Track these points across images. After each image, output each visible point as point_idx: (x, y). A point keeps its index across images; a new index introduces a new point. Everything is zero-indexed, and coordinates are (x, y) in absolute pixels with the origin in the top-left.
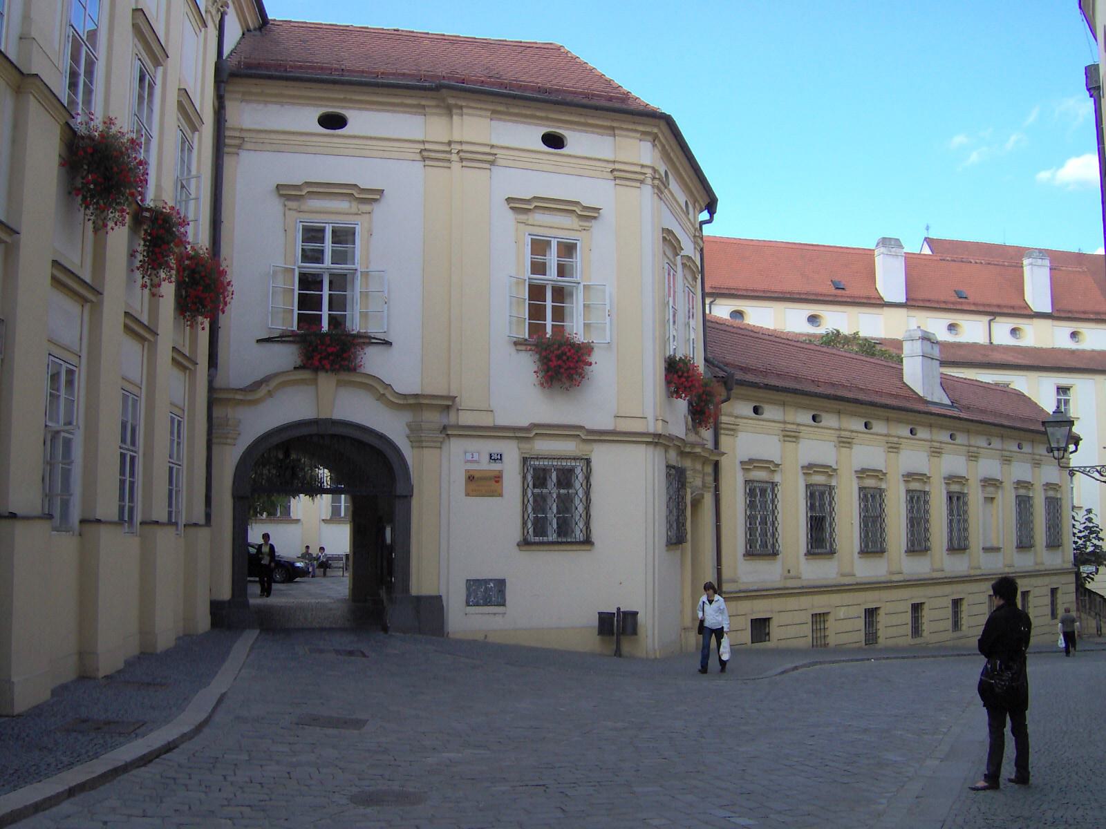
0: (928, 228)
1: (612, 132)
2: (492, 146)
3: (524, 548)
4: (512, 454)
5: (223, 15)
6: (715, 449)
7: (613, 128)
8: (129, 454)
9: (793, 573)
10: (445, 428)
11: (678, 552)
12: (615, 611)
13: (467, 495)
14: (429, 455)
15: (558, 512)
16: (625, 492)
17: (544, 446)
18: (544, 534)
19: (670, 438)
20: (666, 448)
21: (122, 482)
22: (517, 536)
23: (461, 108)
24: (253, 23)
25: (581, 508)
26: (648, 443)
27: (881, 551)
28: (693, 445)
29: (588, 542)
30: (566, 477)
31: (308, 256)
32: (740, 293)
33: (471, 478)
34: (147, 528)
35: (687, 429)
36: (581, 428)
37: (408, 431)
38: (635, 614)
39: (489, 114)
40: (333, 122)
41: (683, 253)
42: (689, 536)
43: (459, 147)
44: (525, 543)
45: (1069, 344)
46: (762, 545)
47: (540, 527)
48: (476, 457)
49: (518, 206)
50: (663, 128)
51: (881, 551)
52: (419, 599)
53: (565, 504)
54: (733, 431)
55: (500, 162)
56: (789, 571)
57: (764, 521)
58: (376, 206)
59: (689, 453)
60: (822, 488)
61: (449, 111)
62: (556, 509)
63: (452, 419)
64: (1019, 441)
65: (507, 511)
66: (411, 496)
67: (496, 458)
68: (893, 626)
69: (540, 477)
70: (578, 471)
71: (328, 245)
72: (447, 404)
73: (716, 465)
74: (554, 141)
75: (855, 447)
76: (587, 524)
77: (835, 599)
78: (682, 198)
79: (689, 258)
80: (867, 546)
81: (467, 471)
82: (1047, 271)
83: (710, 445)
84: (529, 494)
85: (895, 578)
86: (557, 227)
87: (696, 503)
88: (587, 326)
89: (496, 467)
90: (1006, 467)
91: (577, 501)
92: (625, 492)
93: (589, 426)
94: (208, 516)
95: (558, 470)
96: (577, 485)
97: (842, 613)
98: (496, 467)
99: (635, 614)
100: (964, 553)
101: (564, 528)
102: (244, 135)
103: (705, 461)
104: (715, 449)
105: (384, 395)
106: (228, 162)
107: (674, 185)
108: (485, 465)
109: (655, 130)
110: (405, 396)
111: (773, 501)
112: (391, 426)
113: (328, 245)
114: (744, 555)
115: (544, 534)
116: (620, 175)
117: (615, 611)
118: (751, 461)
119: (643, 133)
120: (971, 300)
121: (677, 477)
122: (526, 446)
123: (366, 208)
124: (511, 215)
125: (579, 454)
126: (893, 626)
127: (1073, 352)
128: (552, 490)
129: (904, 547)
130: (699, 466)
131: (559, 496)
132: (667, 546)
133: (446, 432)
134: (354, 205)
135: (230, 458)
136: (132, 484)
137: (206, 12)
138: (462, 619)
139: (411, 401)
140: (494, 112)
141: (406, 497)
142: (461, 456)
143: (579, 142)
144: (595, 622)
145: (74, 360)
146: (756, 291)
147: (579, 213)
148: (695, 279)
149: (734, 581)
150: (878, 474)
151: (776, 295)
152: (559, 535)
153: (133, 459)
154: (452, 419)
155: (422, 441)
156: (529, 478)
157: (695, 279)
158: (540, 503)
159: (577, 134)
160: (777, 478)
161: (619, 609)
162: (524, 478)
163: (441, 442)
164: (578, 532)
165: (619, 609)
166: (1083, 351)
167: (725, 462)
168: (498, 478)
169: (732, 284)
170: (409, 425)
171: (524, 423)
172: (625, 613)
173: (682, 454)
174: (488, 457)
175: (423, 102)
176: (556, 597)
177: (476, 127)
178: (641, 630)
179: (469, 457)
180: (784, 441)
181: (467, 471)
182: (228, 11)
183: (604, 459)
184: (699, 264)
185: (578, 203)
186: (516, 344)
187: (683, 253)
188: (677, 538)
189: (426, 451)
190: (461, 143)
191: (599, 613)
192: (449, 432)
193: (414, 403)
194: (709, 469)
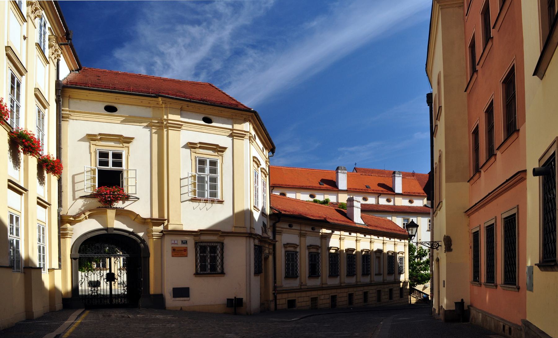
0: (356, 164)
4: (191, 241)
5: (58, 60)
8: (42, 246)
9: (304, 284)
11: (259, 277)
13: (173, 256)
15: (210, 262)
17: (204, 238)
18: (205, 271)
19: (256, 235)
20: (254, 239)
21: (40, 256)
22: (194, 272)
25: (219, 261)
26: (246, 237)
28: (265, 238)
29: (222, 273)
30: (213, 249)
31: (101, 163)
33: (174, 250)
38: (242, 299)
41: (261, 167)
42: (263, 271)
44: (197, 274)
45: (410, 205)
46: (291, 273)
47: (203, 268)
48: (176, 242)
53: (214, 259)
54: (280, 233)
65: (188, 263)
67: (185, 242)
68: (372, 297)
70: (218, 247)
71: (110, 159)
73: (274, 246)
76: (222, 266)
77: (320, 292)
78: (261, 146)
79: (263, 169)
81: (172, 247)
82: (401, 178)
83: (271, 238)
84: (198, 255)
86: (208, 155)
87: (266, 258)
91: (218, 258)
92: (238, 256)
95: (210, 246)
96: (218, 252)
97: (322, 297)
99: (242, 299)
103: (270, 244)
106: (63, 123)
107: (257, 140)
108: (180, 245)
111: (296, 258)
113: (110, 159)
115: (205, 271)
118: (288, 244)
120: (372, 188)
121: (259, 250)
122: (197, 238)
126: (372, 297)
127: (409, 207)
130: (267, 246)
131: (210, 256)
135: (69, 243)
136: (44, 256)
137: (49, 58)
138: (171, 302)
145: (44, 224)
148: (266, 177)
149: (281, 287)
152: (211, 271)
153: (43, 248)
156: (198, 249)
157: (266, 177)
160: (298, 250)
162: (196, 250)
164: (218, 269)
166: (413, 207)
167: (278, 245)
168: (185, 250)
169: (280, 183)
172: (238, 299)
173: (260, 241)
176: (209, 292)
179: (173, 242)
181: (172, 247)
182: (60, 58)
183: (229, 242)
184: (267, 171)
187: (261, 167)
188: (258, 271)
194: (271, 247)
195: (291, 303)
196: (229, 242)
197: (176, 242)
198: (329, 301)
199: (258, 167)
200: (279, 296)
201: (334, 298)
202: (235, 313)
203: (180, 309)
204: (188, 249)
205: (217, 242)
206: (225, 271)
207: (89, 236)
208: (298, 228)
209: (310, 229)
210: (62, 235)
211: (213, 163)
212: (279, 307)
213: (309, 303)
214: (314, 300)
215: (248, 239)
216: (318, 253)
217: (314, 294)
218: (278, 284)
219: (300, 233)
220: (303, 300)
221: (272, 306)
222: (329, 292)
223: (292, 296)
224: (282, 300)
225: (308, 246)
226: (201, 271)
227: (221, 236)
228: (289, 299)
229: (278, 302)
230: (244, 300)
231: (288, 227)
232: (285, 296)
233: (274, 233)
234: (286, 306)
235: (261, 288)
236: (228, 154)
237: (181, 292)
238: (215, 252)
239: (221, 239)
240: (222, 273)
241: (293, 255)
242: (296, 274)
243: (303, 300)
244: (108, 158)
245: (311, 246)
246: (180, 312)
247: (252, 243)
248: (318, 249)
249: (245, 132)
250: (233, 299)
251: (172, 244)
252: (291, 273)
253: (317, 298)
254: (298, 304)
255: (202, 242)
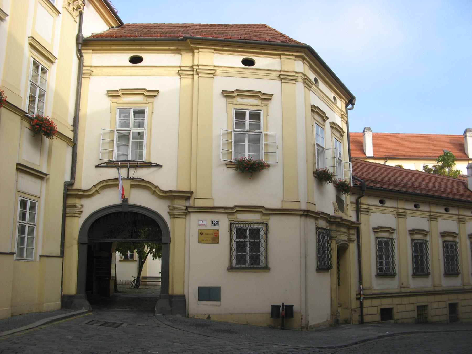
1: (279, 57)
2: (214, 66)
3: (230, 271)
6: (117, 186)
7: (280, 55)
9: (405, 284)
10: (187, 208)
11: (329, 273)
12: (281, 305)
14: (179, 222)
16: (288, 242)
17: (241, 217)
20: (316, 219)
22: (227, 265)
23: (198, 49)
24: (114, 24)
26: (301, 215)
27: (427, 275)
29: (266, 268)
30: (255, 233)
32: (399, 157)
34: (42, 258)
35: (335, 209)
36: (262, 207)
37: (168, 210)
38: (293, 306)
39: (213, 51)
40: (136, 60)
43: (197, 68)
44: (231, 268)
46: (385, 270)
47: (241, 259)
48: (204, 223)
49: (227, 95)
50: (307, 53)
51: (427, 275)
52: (172, 296)
53: (255, 247)
54: (367, 212)
55: (217, 74)
56: (402, 284)
57: (387, 257)
58: (156, 99)
59: (333, 221)
60: (452, 243)
61: (192, 51)
62: (249, 249)
63: (191, 203)
64: (445, 207)
65: (222, 250)
66: (170, 243)
69: (241, 233)
72: (187, 196)
73: (358, 229)
74: (248, 62)
75: (439, 220)
76: (266, 257)
77: (431, 298)
80: (448, 271)
81: (199, 230)
85: (437, 289)
86: (248, 104)
88: (266, 154)
89: (216, 228)
90: (401, 220)
92: (288, 242)
93: (266, 206)
94: (62, 252)
97: (435, 305)
98: (216, 228)
99: (293, 306)
100: (457, 277)
101: (255, 260)
102: (93, 69)
104: (117, 186)
105: (155, 191)
106: (84, 81)
107: (321, 85)
109: (303, 54)
110: (165, 192)
112: (160, 207)
114: (376, 276)
116: (283, 77)
117: (281, 305)
118: (379, 228)
119: (296, 56)
121: (323, 237)
122: (232, 217)
123: (150, 100)
124: (224, 100)
125: (261, 221)
128: (248, 240)
129: (410, 272)
132: (316, 270)
133: (188, 211)
134: (145, 98)
135: (76, 225)
138: (196, 307)
139: (168, 194)
140: (215, 50)
141: (167, 243)
142: (197, 222)
143: (261, 61)
144: (269, 310)
146: (406, 156)
147: (261, 97)
150: (453, 235)
151: (416, 157)
154: (191, 203)
155: (174, 215)
158: (241, 247)
159: (260, 59)
160: (428, 238)
161: (283, 304)
163: (185, 215)
165: (283, 304)
167: (363, 228)
170: (169, 207)
171: (231, 205)
172: (287, 306)
174: (211, 223)
175: (180, 48)
176: (248, 296)
177: (207, 57)
178: (295, 315)
180: (398, 217)
181: (199, 230)
183: (275, 223)
185: (260, 92)
186: (226, 164)
188: (323, 267)
189: (177, 220)
190: (198, 65)
191: (272, 306)
192: (189, 210)
193: (170, 196)
195: (386, 314)
196: (275, 223)
197: (204, 223)
198: (447, 311)
199: (324, 121)
200: (366, 303)
201: (453, 307)
202: (283, 328)
203: (207, 316)
204: (220, 233)
205: (260, 223)
206: (270, 265)
207: (100, 215)
208: (456, 212)
209: (443, 211)
210: (67, 212)
211: (255, 116)
212: (367, 319)
213: (415, 314)
214: (422, 309)
215: (303, 219)
216: (456, 243)
217: (422, 300)
218: (366, 284)
219: (398, 212)
220: (404, 309)
221: (356, 317)
222: (445, 297)
223: (386, 303)
224: (372, 309)
225: (410, 231)
226: (237, 263)
227: (265, 214)
228: (383, 307)
229: (365, 311)
230: (296, 308)
231: (378, 204)
232: (376, 302)
233: (358, 211)
234: (377, 318)
235: (331, 291)
236: (274, 104)
237: (209, 294)
238: (244, 237)
239: (265, 218)
240: (266, 268)
241: (421, 244)
242: (457, 270)
243: (404, 309)
244: (244, 142)
245: (445, 233)
246: (205, 324)
247: (311, 225)
248: (426, 235)
249: (296, 73)
250: (279, 306)
251: (199, 225)
252: (385, 270)
253: (426, 306)
254: (397, 316)
255: (239, 224)
